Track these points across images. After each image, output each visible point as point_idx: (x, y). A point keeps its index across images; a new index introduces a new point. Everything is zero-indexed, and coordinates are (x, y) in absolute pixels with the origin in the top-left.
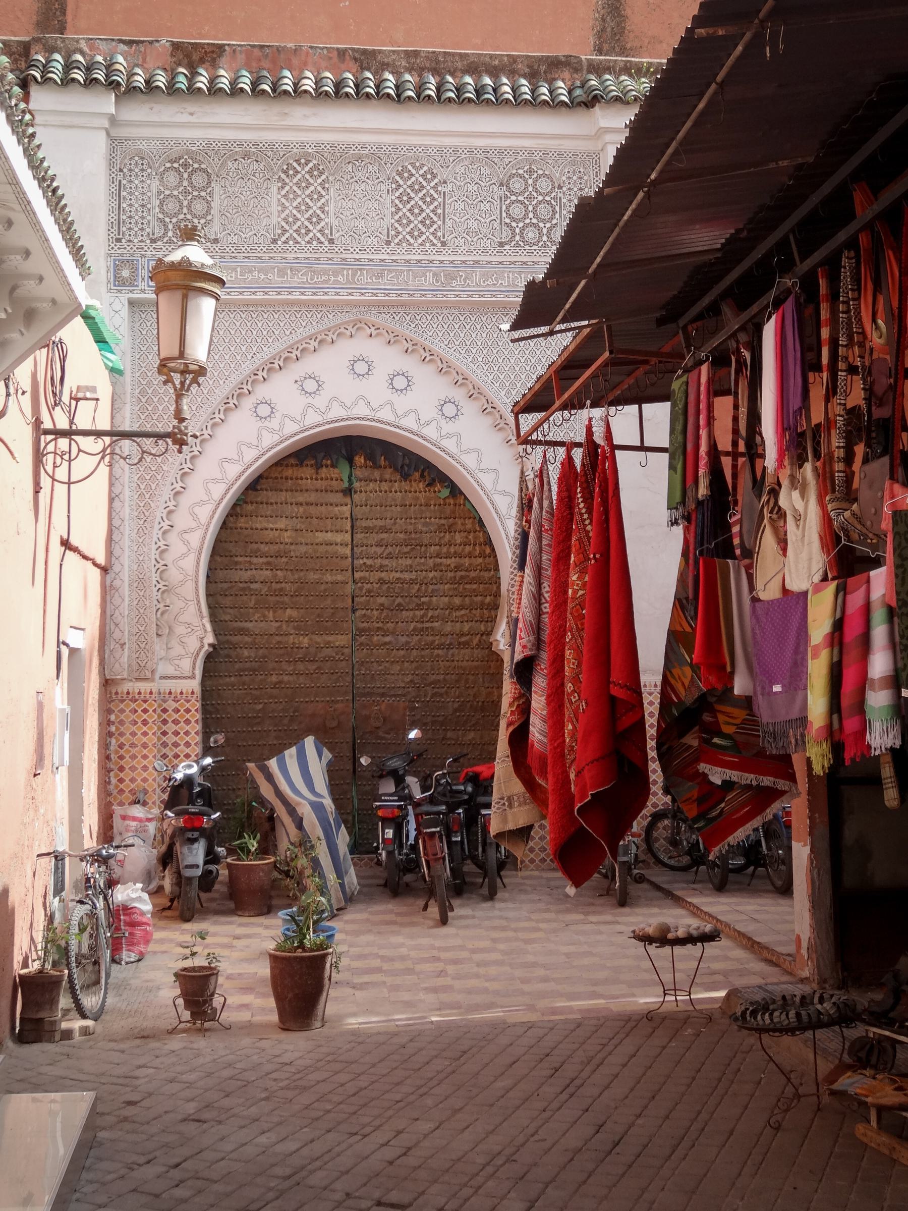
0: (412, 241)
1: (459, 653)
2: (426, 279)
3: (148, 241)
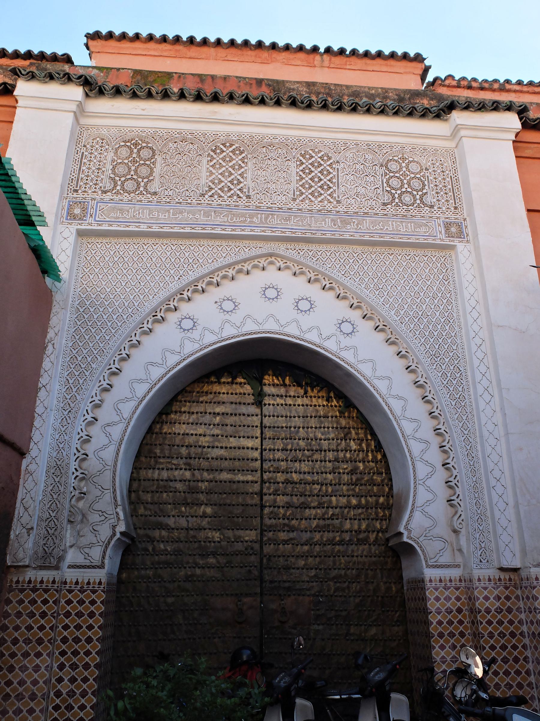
0: (313, 199)
1: (358, 549)
2: (325, 223)
3: (100, 192)
